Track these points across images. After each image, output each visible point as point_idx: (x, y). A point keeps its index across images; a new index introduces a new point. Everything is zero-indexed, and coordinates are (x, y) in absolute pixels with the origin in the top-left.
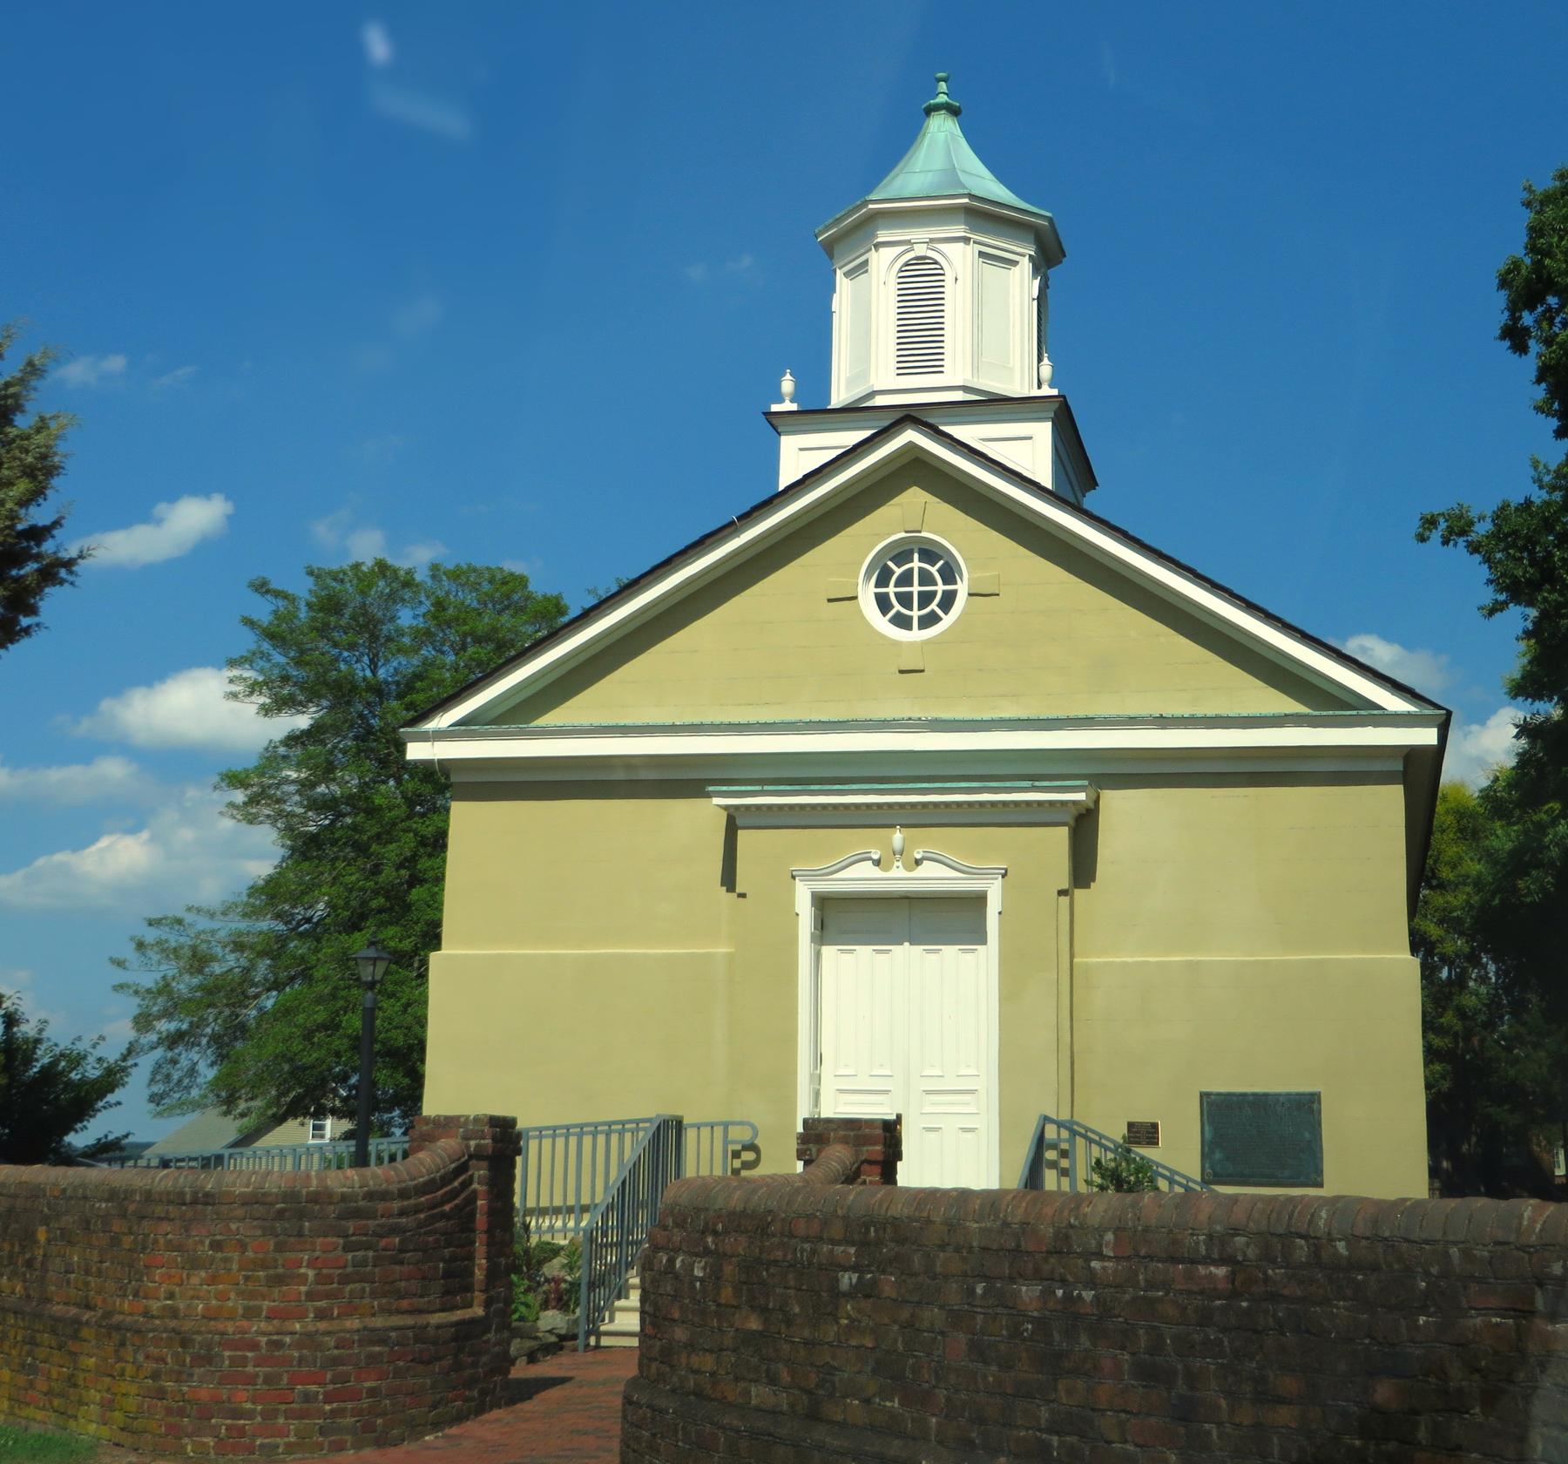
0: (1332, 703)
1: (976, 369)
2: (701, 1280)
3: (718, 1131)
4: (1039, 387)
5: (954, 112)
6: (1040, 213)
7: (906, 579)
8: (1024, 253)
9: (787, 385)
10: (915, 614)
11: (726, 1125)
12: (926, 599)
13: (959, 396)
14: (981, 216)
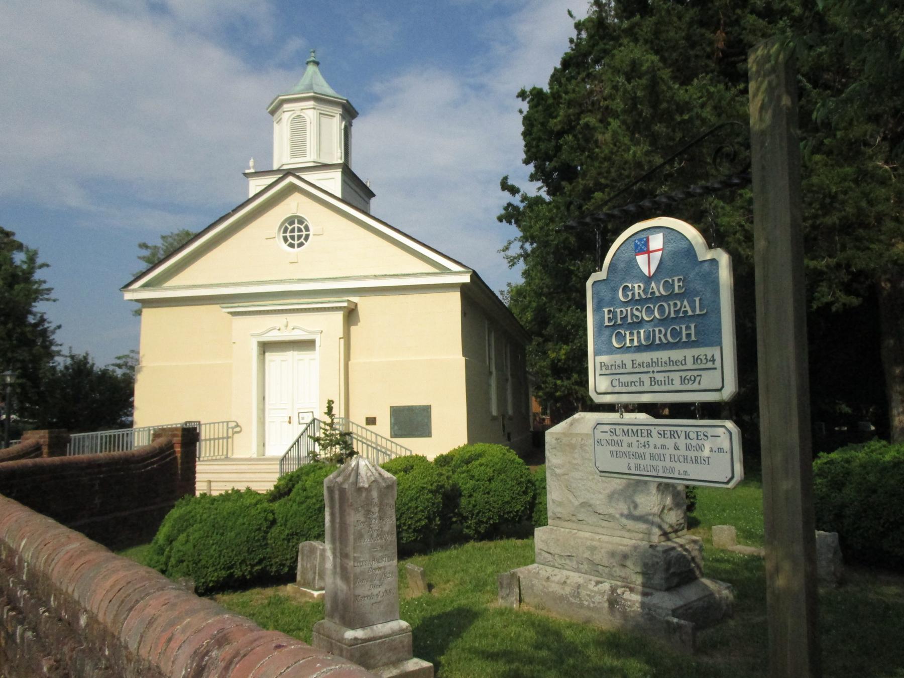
0: (444, 270)
1: (319, 155)
2: (11, 385)
3: (225, 424)
4: (715, 369)
5: (317, 63)
6: (342, 98)
7: (293, 231)
8: (338, 111)
9: (251, 163)
10: (296, 242)
11: (228, 422)
12: (299, 237)
13: (312, 164)
14: (319, 99)
